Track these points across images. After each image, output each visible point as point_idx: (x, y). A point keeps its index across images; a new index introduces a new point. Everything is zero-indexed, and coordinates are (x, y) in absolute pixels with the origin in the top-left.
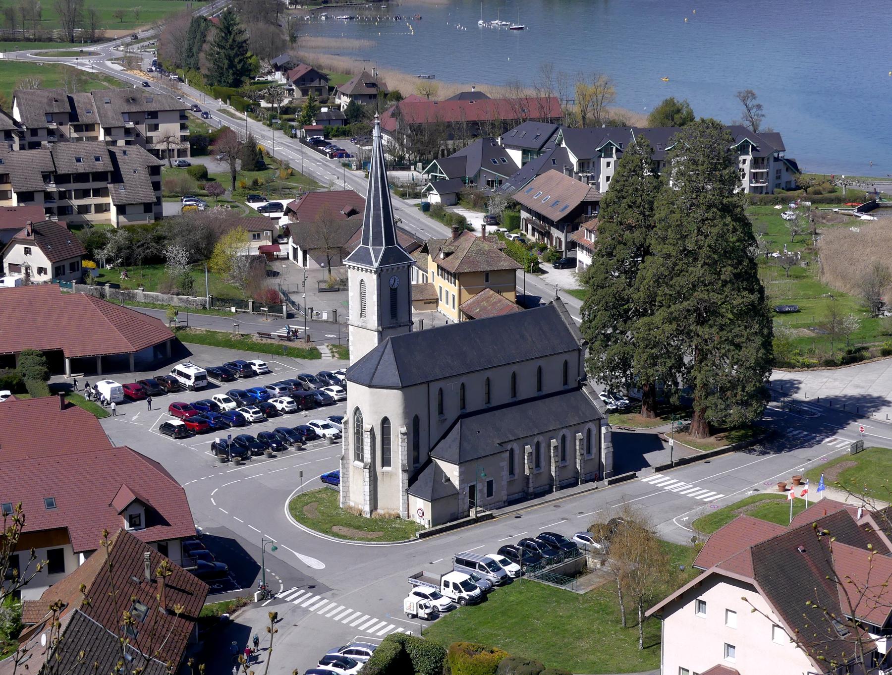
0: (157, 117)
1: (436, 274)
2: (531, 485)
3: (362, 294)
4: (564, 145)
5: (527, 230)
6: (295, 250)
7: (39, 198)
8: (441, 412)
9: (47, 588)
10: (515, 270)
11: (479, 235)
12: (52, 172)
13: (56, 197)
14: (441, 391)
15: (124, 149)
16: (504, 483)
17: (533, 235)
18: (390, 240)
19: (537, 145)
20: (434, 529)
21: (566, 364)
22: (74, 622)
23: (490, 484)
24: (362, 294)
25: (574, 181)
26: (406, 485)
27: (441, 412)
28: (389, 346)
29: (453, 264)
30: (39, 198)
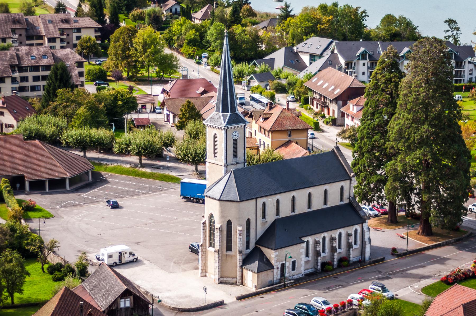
0: (80, 32)
4: (336, 52)
5: (313, 105)
6: (168, 116)
7: (58, 41)
8: (264, 217)
11: (286, 107)
12: (17, 65)
13: (19, 80)
14: (264, 204)
15: (71, 43)
16: (303, 263)
17: (317, 107)
18: (233, 109)
19: (319, 52)
20: (257, 290)
21: (342, 188)
23: (294, 263)
25: (342, 74)
26: (241, 263)
27: (264, 217)
30: (58, 41)
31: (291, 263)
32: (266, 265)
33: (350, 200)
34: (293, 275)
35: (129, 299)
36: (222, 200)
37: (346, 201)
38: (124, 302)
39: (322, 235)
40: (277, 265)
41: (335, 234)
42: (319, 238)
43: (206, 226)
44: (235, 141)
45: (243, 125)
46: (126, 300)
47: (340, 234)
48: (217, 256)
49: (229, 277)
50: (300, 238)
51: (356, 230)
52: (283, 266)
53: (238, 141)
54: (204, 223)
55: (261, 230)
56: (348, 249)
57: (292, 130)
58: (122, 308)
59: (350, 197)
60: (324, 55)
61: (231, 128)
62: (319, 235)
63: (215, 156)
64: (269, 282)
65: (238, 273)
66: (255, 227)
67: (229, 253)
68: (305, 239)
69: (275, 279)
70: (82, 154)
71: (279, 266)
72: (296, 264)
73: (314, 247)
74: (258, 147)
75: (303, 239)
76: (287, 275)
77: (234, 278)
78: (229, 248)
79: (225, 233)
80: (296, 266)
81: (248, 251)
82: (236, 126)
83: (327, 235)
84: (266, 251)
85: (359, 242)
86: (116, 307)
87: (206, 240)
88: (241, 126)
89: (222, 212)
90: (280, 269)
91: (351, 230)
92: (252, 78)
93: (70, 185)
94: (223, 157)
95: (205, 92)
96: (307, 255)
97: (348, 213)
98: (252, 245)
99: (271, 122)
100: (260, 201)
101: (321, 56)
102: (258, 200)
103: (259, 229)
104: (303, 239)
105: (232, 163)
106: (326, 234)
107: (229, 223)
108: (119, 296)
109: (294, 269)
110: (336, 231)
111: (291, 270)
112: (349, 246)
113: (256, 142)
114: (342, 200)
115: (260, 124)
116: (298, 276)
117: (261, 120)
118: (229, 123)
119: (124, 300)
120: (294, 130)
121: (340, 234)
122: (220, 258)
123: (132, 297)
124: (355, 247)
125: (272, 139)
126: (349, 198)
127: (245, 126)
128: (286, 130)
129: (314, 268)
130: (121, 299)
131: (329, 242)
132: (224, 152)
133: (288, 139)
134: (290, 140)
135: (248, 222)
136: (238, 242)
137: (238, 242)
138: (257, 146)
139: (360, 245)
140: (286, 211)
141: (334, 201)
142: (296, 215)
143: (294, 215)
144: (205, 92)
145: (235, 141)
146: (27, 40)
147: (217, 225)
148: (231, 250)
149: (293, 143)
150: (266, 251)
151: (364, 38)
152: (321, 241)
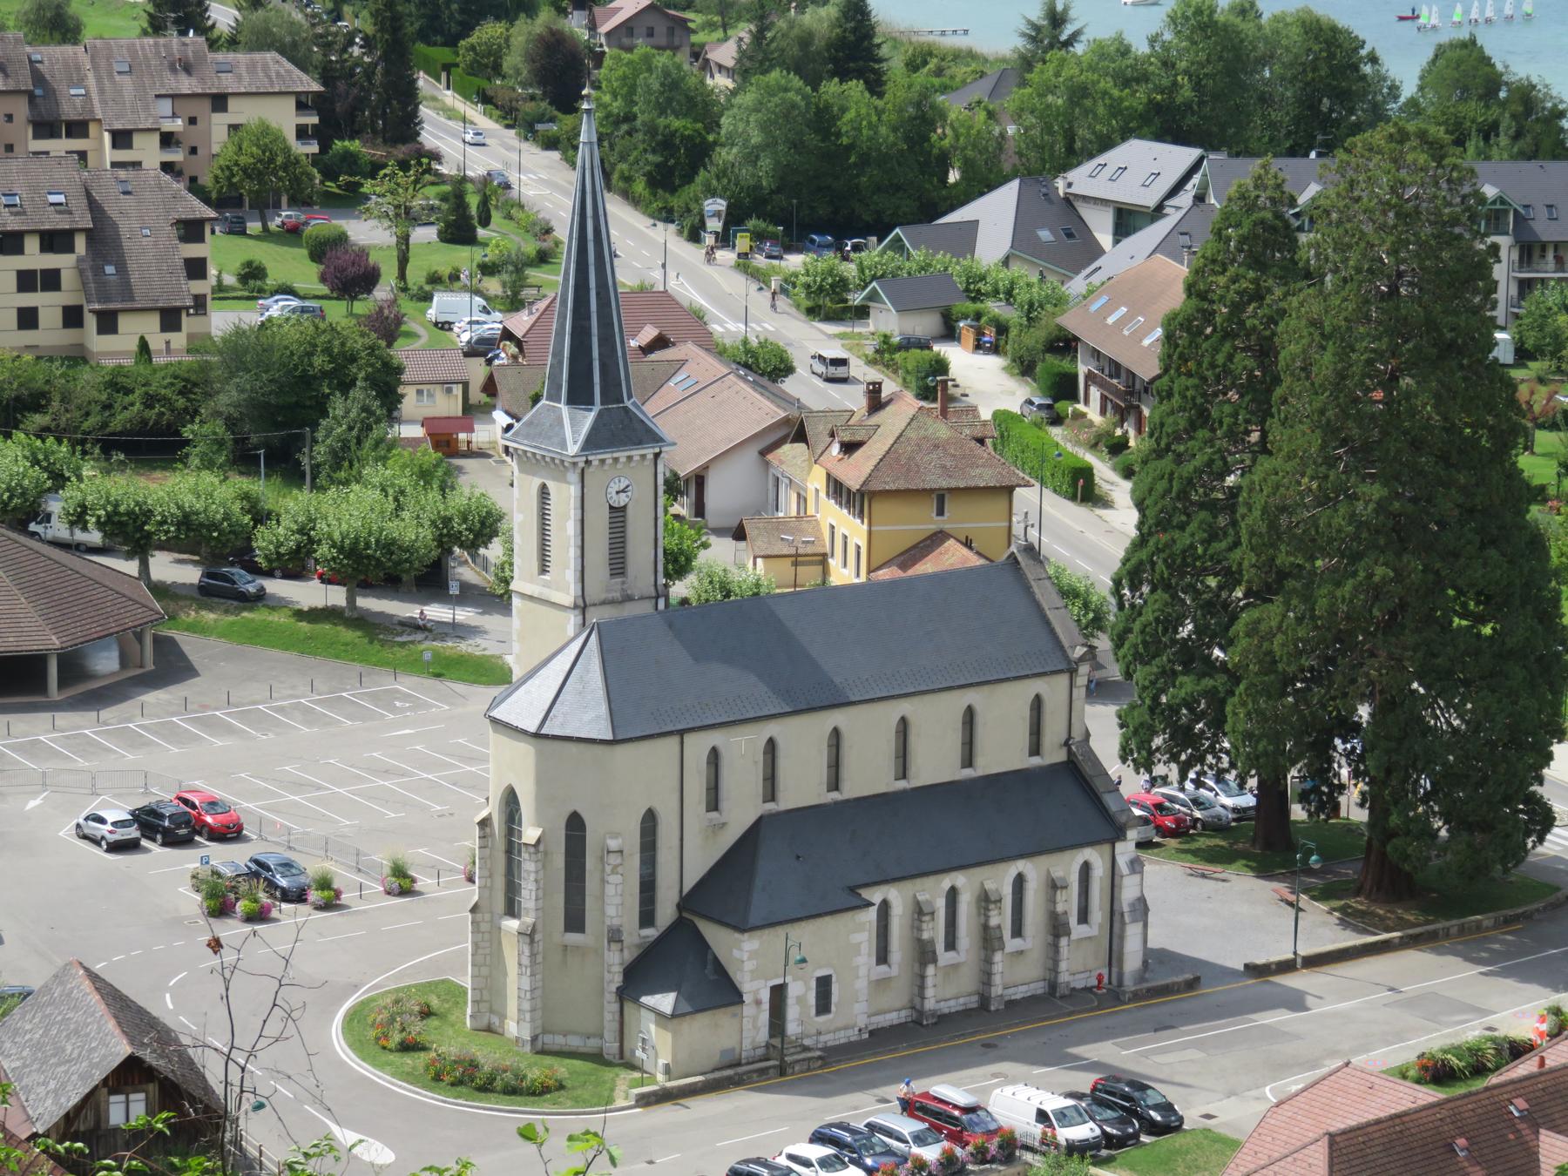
1: (823, 494)
2: (930, 992)
3: (858, 554)
5: (1087, 402)
8: (713, 804)
9: (1356, 1060)
10: (1009, 490)
14: (714, 756)
16: (861, 984)
17: (1103, 412)
21: (1037, 704)
22: (1430, 1112)
23: (824, 984)
24: (858, 554)
27: (713, 804)
28: (594, 637)
29: (855, 472)
31: (813, 984)
32: (718, 990)
33: (1070, 751)
34: (819, 1033)
35: (142, 1096)
36: (546, 737)
37: (1053, 755)
38: (123, 1106)
39: (946, 882)
40: (756, 992)
41: (1000, 879)
42: (932, 891)
43: (492, 835)
44: (618, 514)
45: (650, 452)
46: (132, 1097)
47: (1020, 881)
48: (527, 952)
49: (574, 1033)
50: (853, 890)
51: (1086, 869)
52: (778, 993)
53: (630, 512)
54: (484, 823)
55: (700, 859)
56: (1050, 939)
57: (950, 490)
58: (116, 1130)
59: (1070, 737)
60: (1167, 210)
61: (603, 461)
62: (929, 882)
63: (543, 570)
64: (724, 1053)
65: (608, 1017)
66: (676, 842)
67: (574, 938)
68: (876, 895)
69: (747, 1045)
70: (131, 567)
71: (765, 996)
72: (835, 988)
73: (912, 927)
74: (824, 555)
75: (866, 894)
76: (792, 1028)
77: (594, 1036)
78: (575, 920)
79: (559, 861)
80: (834, 998)
81: (651, 933)
82: (622, 455)
83: (965, 882)
84: (717, 937)
85: (1098, 914)
86: (91, 1123)
87: (491, 889)
88: (643, 457)
89: (543, 779)
90: (766, 1006)
91: (1067, 866)
92: (873, 296)
93: (63, 683)
94: (570, 576)
95: (661, 343)
96: (883, 957)
97: (1067, 800)
98: (666, 912)
99: (869, 457)
100: (698, 746)
101: (1158, 212)
102: (689, 739)
103: (692, 854)
104: (866, 894)
105: (603, 596)
106: (959, 879)
107: (575, 824)
108: (105, 1081)
109: (823, 1005)
110: (1002, 866)
111: (813, 1011)
112: (1057, 927)
113: (820, 538)
114: (1035, 750)
115: (829, 465)
116: (841, 1038)
117: (835, 449)
118: (593, 442)
119: (122, 1098)
120: (958, 489)
121: (1020, 881)
122: (539, 959)
123: (153, 1088)
124: (1078, 931)
125: (870, 525)
126: (1067, 744)
127: (657, 456)
128: (924, 490)
129: (913, 1008)
130: (114, 1091)
131: (974, 911)
132: (573, 553)
133: (933, 527)
134: (941, 532)
135: (650, 821)
136: (614, 898)
137: (614, 898)
138: (820, 550)
139: (1101, 926)
140: (803, 786)
141: (1003, 751)
142: (847, 801)
143: (836, 803)
144: (661, 343)
145: (618, 514)
146: (36, 136)
147: (530, 834)
148: (819, 980)
149: (951, 542)
150: (717, 937)
151: (1321, 146)
152: (941, 904)
